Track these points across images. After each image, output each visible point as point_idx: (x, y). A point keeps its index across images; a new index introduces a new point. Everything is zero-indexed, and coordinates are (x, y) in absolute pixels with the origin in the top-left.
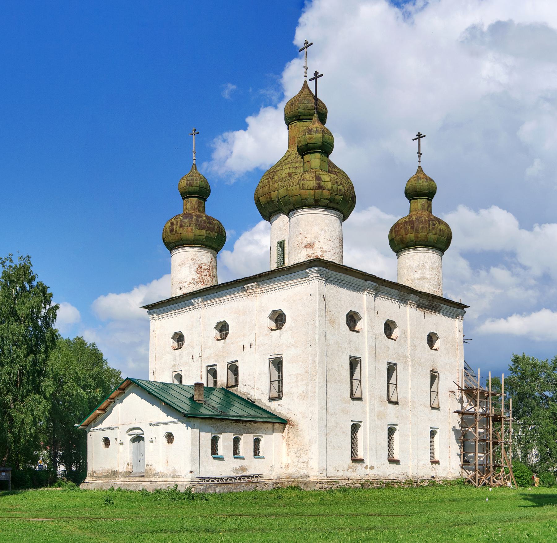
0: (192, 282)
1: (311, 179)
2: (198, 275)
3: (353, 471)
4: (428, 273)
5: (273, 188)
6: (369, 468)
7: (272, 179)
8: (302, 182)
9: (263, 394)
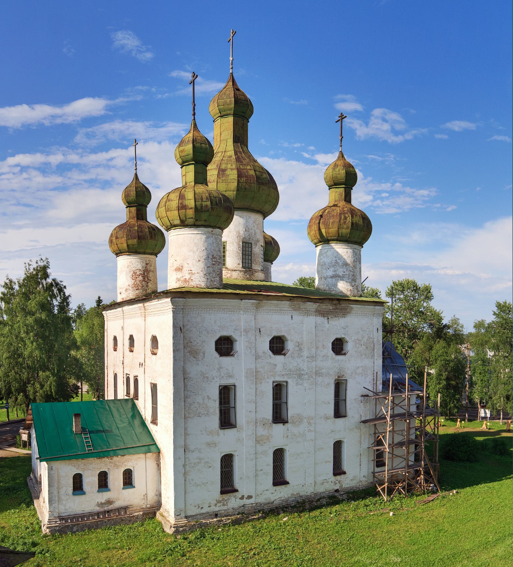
0: (128, 287)
2: (133, 281)
3: (224, 505)
4: (341, 270)
6: (245, 498)
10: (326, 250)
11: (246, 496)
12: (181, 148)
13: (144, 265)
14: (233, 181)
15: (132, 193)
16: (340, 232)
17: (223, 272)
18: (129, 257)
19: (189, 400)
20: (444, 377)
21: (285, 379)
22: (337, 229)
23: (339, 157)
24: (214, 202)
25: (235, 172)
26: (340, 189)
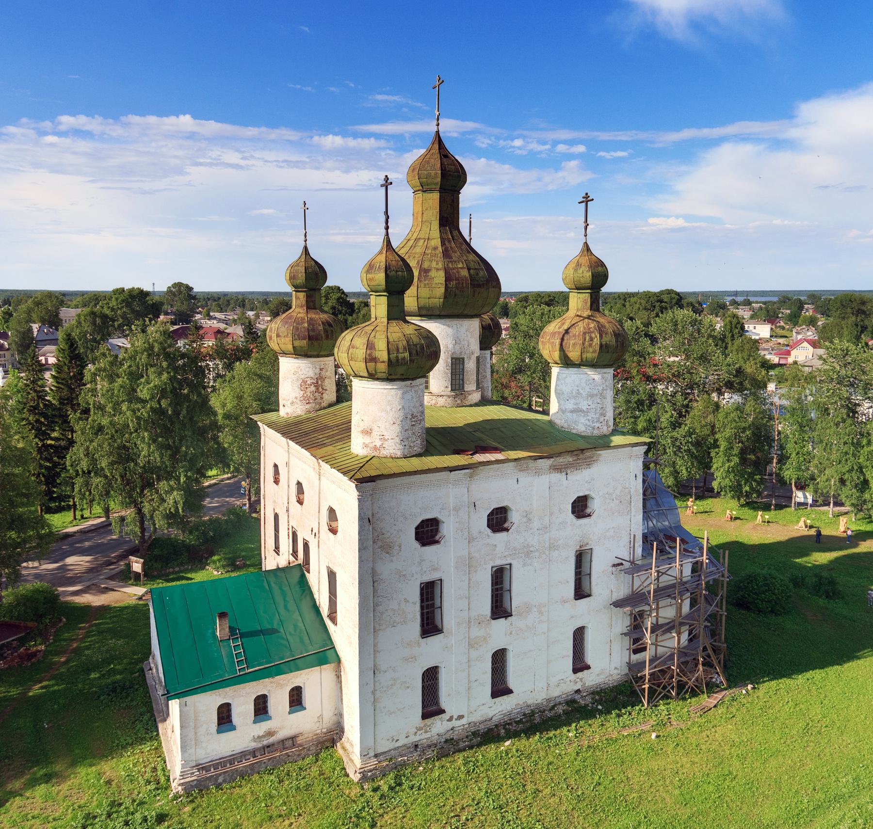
2: (302, 393)
3: (426, 732)
4: (585, 403)
10: (564, 376)
11: (455, 717)
12: (370, 276)
13: (318, 371)
14: (440, 286)
16: (584, 356)
17: (425, 397)
18: (296, 361)
19: (380, 608)
20: (736, 451)
21: (508, 562)
22: (579, 353)
23: (582, 251)
24: (414, 352)
25: (442, 274)
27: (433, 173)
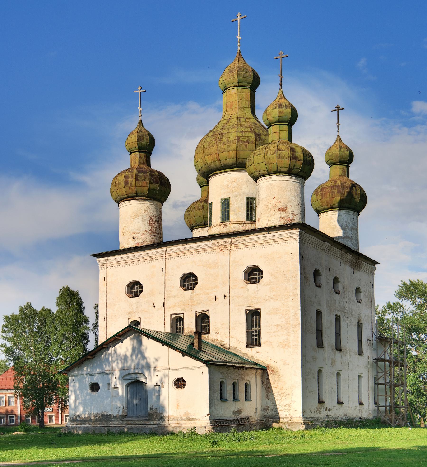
0: (145, 233)
1: (286, 150)
2: (150, 227)
4: (350, 233)
5: (221, 150)
7: (220, 140)
8: (279, 152)
9: (238, 342)
15: (145, 139)
26: (343, 166)
27: (248, 74)
